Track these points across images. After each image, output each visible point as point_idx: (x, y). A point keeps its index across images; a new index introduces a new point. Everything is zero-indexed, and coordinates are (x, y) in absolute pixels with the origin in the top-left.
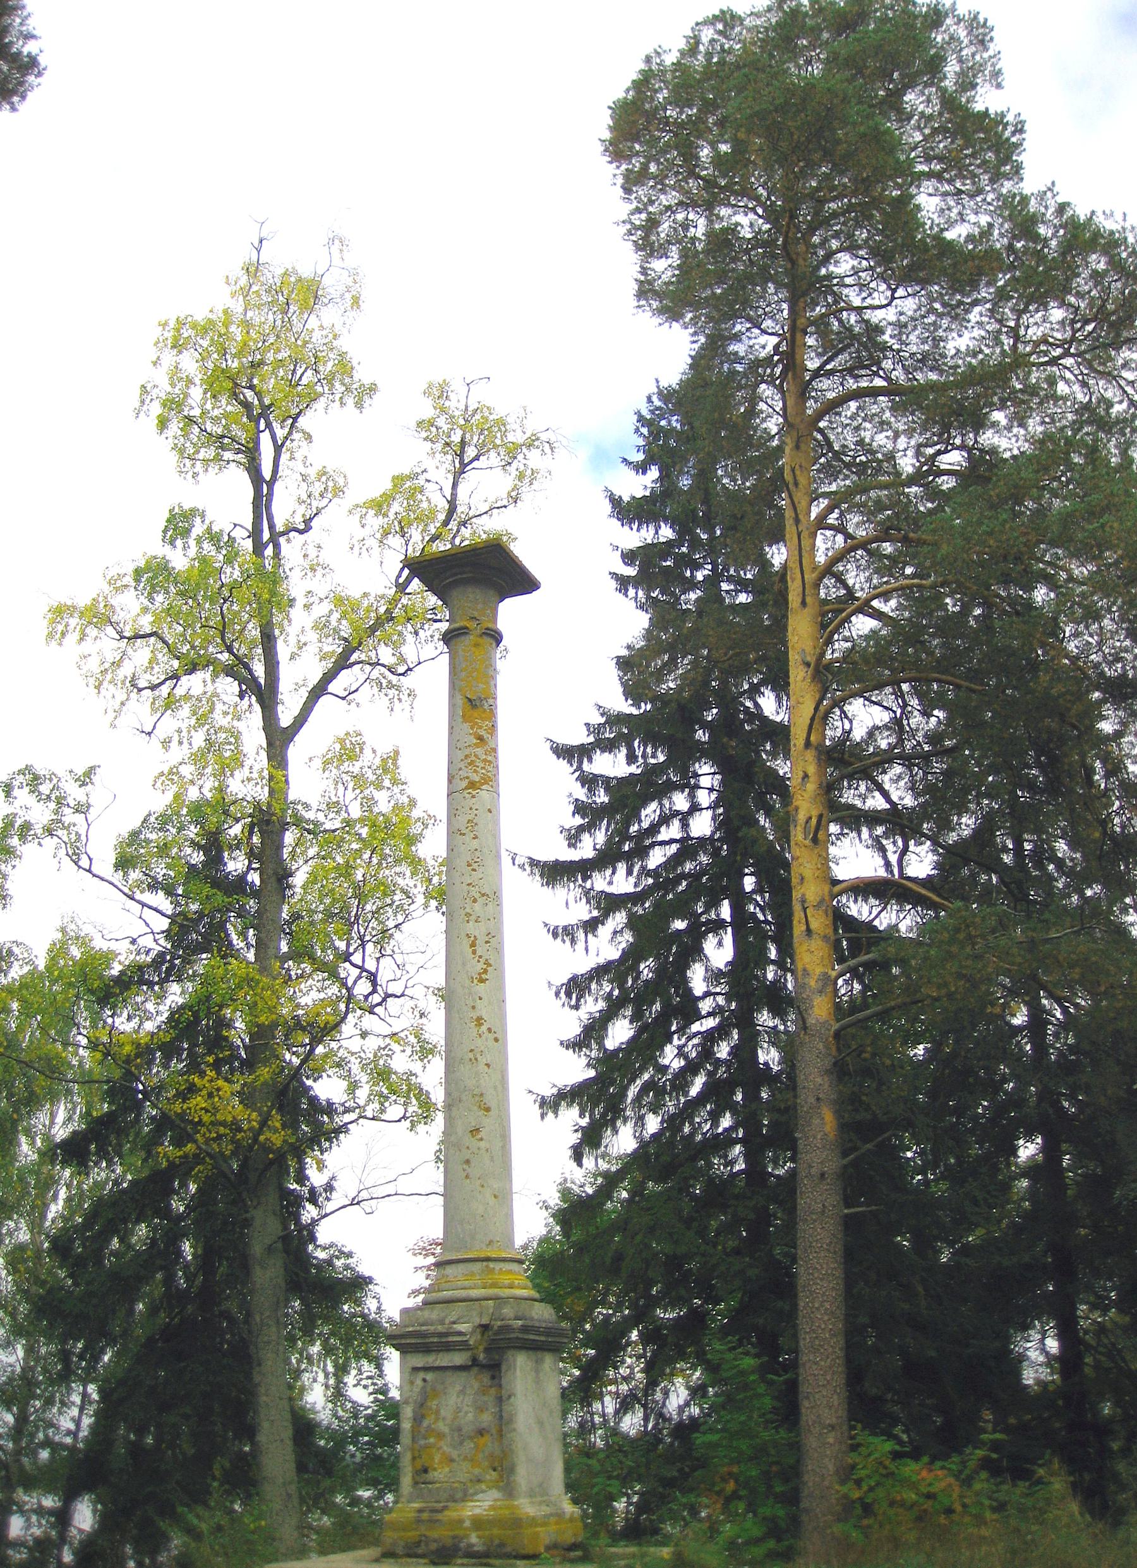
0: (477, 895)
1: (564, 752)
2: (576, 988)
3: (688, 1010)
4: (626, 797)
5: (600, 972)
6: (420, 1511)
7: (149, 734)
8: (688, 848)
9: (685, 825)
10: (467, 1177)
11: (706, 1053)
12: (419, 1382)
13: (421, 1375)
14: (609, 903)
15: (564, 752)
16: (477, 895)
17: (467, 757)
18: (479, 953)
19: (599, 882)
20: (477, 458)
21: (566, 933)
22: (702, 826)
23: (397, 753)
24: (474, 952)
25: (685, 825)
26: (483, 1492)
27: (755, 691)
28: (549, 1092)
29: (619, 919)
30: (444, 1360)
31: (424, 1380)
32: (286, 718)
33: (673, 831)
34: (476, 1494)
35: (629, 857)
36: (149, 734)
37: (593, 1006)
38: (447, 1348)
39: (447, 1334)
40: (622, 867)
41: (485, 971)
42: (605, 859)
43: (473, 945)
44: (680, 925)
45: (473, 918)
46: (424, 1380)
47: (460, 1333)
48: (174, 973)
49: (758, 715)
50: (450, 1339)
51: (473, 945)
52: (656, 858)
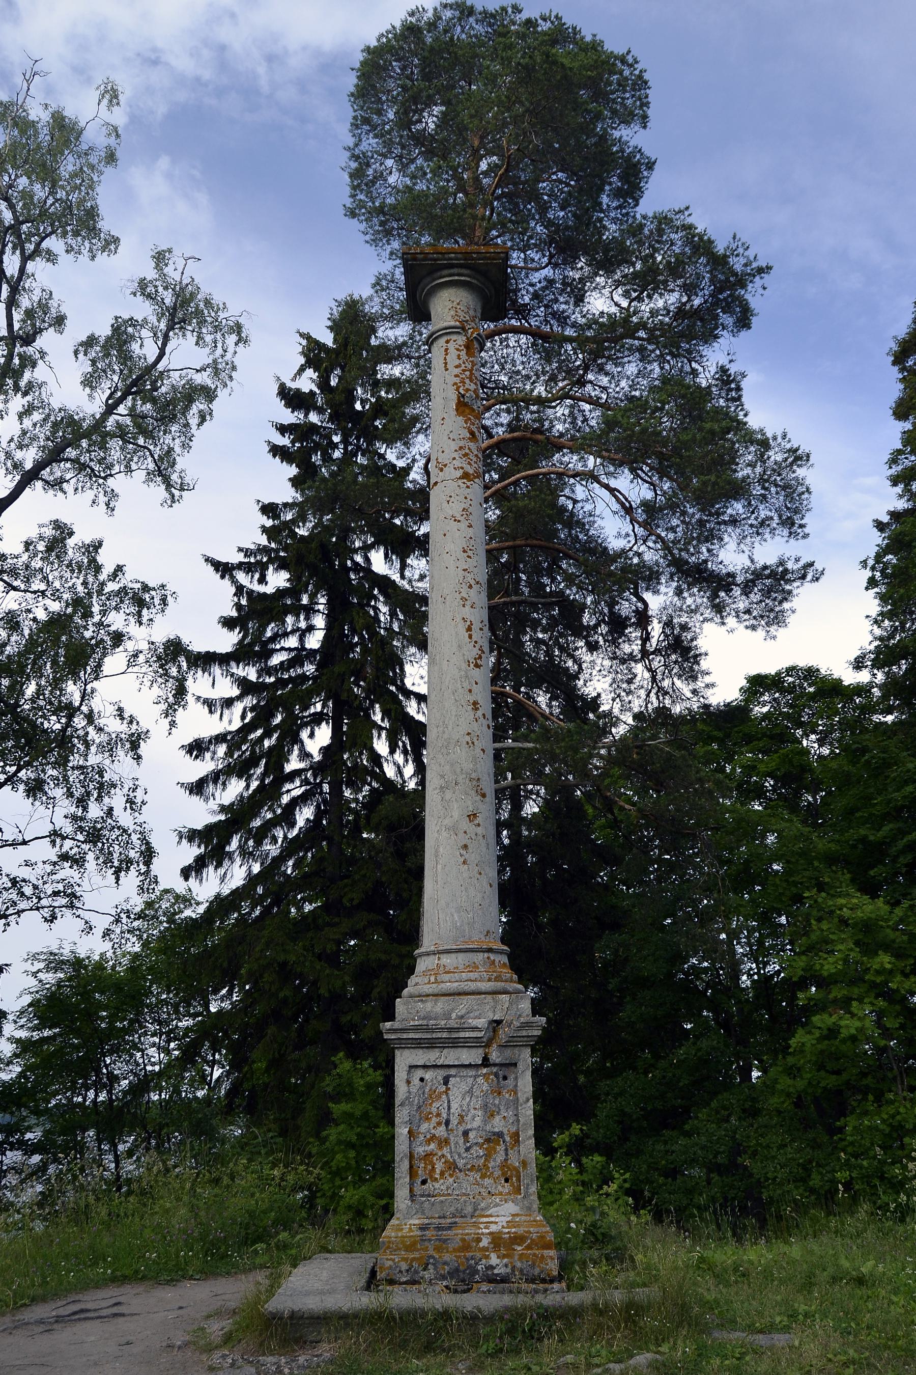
0: (473, 582)
1: (224, 569)
2: (197, 748)
5: (220, 738)
6: (423, 1228)
8: (300, 656)
9: (302, 640)
10: (464, 862)
12: (416, 1081)
13: (420, 1073)
14: (246, 687)
15: (224, 569)
16: (473, 582)
17: (461, 448)
18: (474, 638)
22: (314, 641)
23: (100, 544)
24: (470, 637)
25: (302, 640)
26: (497, 1205)
27: (366, 548)
29: (249, 701)
30: (450, 1057)
31: (422, 1080)
33: (292, 642)
34: (488, 1208)
38: (454, 1044)
39: (458, 1030)
41: (480, 657)
42: (240, 654)
43: (469, 629)
45: (468, 603)
46: (422, 1080)
47: (475, 1029)
49: (367, 571)
50: (462, 1035)
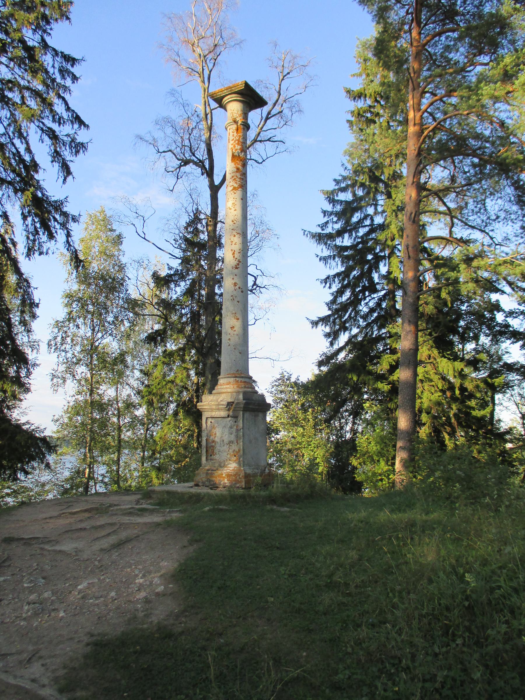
2: (327, 280)
3: (372, 288)
4: (349, 209)
5: (338, 275)
7: (172, 191)
11: (379, 304)
19: (338, 242)
20: (288, 73)
21: (324, 259)
28: (316, 319)
32: (217, 182)
33: (368, 222)
35: (350, 232)
36: (172, 191)
37: (335, 287)
40: (346, 235)
44: (370, 257)
45: (234, 243)
48: (183, 277)
51: (234, 254)
52: (362, 232)
